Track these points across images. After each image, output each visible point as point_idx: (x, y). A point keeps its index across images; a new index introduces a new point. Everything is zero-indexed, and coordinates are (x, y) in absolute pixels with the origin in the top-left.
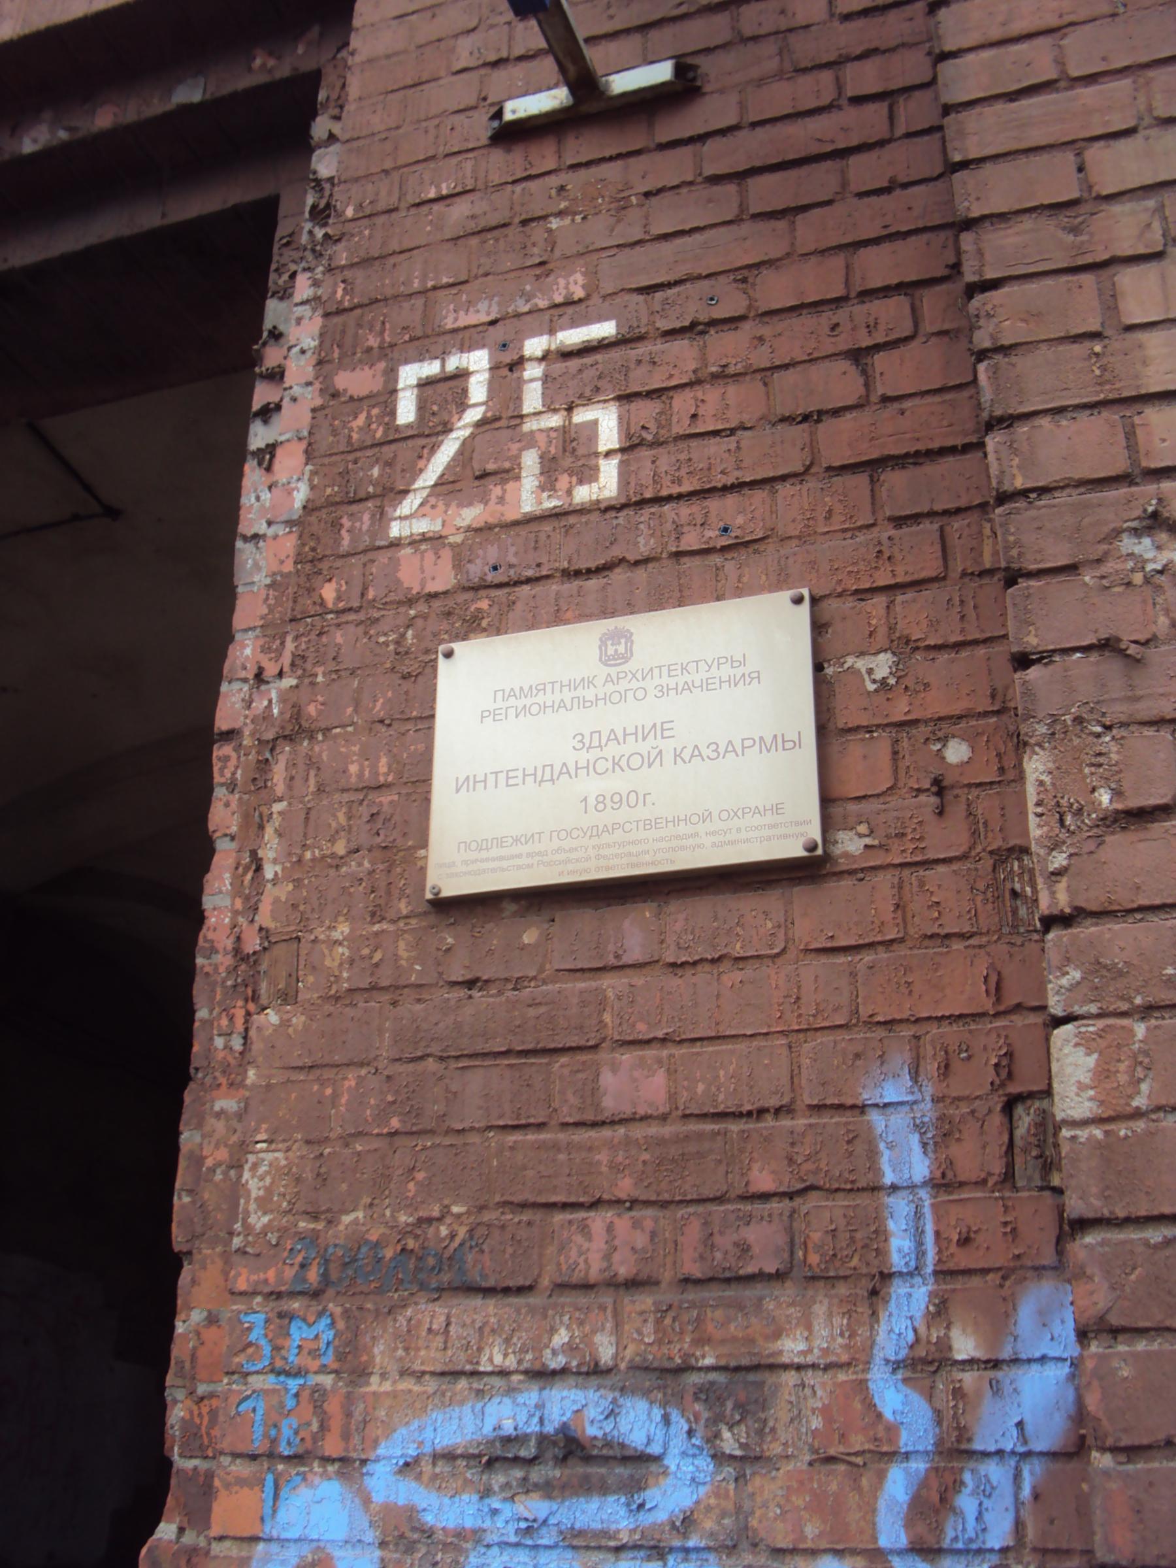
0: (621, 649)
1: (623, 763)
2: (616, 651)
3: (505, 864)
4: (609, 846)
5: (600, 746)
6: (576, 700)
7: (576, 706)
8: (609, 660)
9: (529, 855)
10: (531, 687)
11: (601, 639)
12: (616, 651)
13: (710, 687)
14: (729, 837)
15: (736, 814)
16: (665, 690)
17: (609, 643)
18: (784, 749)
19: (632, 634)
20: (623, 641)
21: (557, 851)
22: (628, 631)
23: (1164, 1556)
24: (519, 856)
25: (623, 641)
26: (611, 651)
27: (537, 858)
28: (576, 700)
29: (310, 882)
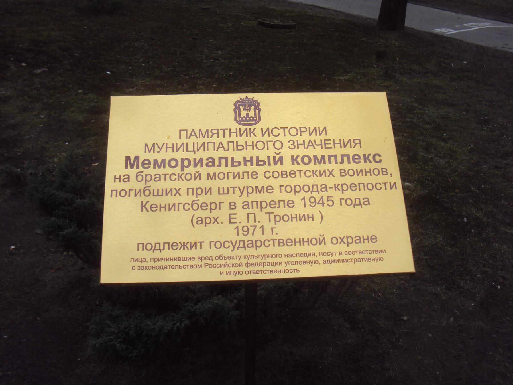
0: (252, 113)
2: (247, 115)
3: (181, 263)
4: (255, 257)
5: (194, 151)
6: (231, 144)
8: (242, 120)
9: (199, 258)
10: (207, 130)
11: (235, 104)
12: (247, 115)
13: (327, 146)
14: (334, 257)
15: (342, 240)
16: (296, 144)
17: (242, 108)
19: (259, 104)
20: (252, 108)
21: (219, 258)
24: (193, 259)
25: (252, 108)
26: (243, 114)
27: (205, 261)
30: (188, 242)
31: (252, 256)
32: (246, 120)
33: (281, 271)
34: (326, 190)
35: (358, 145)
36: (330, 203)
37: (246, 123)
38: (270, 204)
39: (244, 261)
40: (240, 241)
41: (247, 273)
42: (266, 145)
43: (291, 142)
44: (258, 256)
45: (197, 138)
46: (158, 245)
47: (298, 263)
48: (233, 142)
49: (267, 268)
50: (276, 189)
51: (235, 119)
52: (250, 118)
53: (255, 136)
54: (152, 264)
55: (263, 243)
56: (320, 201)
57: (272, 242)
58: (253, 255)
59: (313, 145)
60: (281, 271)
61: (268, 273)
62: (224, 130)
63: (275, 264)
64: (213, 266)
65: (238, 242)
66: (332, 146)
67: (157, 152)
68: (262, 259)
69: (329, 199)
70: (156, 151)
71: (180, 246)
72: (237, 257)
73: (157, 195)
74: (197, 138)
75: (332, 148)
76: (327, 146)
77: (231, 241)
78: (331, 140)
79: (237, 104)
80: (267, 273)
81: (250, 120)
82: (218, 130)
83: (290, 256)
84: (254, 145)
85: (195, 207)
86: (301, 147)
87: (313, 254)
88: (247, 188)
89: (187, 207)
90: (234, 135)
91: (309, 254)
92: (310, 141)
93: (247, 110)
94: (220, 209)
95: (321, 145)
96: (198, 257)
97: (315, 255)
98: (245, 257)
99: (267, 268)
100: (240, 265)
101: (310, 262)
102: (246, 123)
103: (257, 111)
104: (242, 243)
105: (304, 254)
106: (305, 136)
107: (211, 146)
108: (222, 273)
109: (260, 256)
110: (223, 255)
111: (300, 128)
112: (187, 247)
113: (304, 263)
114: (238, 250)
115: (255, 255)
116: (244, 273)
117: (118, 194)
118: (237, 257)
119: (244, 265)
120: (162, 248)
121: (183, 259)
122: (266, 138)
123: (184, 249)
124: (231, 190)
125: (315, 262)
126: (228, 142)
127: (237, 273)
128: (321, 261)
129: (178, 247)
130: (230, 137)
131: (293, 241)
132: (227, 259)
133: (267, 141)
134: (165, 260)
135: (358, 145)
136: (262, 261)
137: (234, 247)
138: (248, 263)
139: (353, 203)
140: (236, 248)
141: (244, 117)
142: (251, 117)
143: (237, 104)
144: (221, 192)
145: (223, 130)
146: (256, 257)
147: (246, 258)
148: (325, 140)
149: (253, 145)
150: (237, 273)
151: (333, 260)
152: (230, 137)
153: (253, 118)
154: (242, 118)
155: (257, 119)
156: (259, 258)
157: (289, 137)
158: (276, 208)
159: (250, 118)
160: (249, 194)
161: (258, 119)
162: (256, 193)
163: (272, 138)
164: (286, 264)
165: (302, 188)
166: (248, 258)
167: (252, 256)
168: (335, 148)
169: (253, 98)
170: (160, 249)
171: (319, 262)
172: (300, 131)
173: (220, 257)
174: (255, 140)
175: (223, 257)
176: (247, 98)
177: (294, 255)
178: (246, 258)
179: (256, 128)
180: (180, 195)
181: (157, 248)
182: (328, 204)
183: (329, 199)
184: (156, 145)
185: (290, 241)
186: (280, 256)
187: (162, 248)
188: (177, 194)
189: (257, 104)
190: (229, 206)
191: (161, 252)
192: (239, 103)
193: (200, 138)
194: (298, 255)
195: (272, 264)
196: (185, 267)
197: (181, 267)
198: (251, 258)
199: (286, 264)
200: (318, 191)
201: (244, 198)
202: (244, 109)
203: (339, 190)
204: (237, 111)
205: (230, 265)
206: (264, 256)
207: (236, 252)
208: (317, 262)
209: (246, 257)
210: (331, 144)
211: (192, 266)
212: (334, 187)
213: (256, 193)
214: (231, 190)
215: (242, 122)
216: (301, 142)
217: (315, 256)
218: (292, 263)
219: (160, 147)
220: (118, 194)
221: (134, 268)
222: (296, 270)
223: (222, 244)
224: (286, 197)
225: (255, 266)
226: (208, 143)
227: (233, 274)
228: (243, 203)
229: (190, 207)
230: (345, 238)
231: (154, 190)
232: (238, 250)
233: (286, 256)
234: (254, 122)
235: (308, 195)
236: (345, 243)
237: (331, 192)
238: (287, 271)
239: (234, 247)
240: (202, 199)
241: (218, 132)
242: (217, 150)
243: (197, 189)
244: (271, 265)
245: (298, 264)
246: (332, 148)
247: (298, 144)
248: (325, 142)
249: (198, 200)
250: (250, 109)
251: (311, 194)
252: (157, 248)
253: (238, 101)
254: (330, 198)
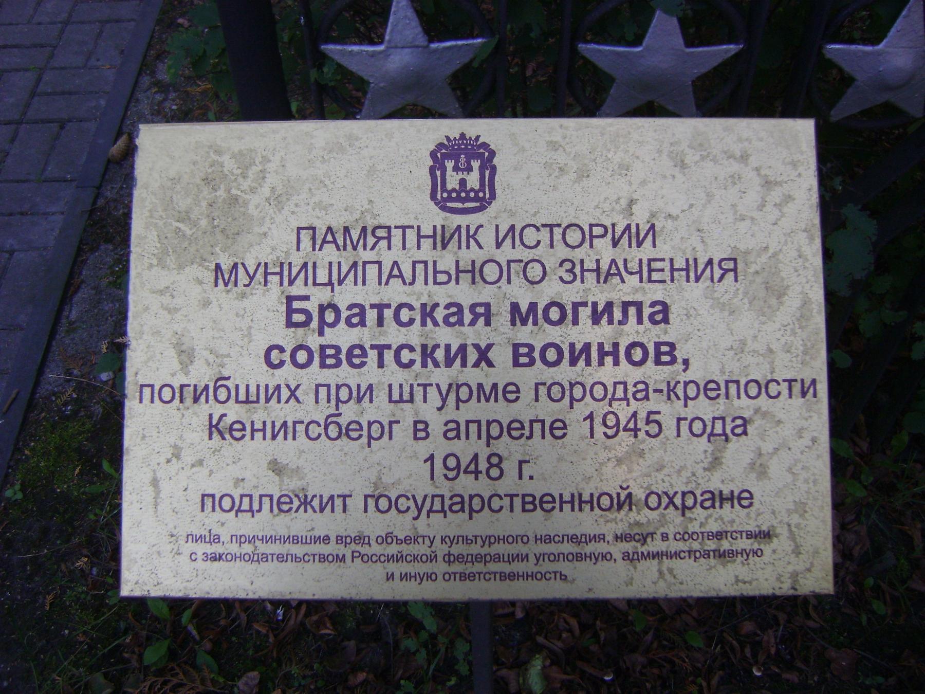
0: (473, 180)
1: (665, 500)
2: (463, 182)
5: (330, 283)
6: (420, 268)
7: (420, 278)
8: (450, 199)
11: (433, 155)
12: (463, 182)
17: (450, 164)
18: (435, 283)
19: (493, 154)
22: (485, 145)
23: (431, 613)
25: (476, 164)
26: (453, 181)
27: (353, 546)
28: (420, 268)
29: (33, 450)
30: (315, 496)
31: (460, 539)
32: (459, 199)
33: (527, 576)
34: (647, 398)
35: (731, 275)
36: (654, 429)
37: (459, 205)
38: (509, 429)
39: (441, 549)
40: (433, 496)
41: (447, 577)
42: (505, 273)
43: (568, 266)
44: (473, 539)
46: (246, 500)
47: (566, 557)
48: (425, 263)
49: (493, 567)
50: (527, 394)
51: (433, 196)
52: (467, 193)
53: (480, 247)
54: (234, 548)
55: (486, 503)
56: (628, 422)
57: (507, 500)
58: (463, 537)
59: (619, 274)
60: (527, 576)
61: (495, 580)
62: (404, 228)
63: (511, 560)
64: (370, 558)
65: (429, 500)
66: (666, 275)
67: (245, 286)
68: (482, 547)
69: (650, 419)
70: (240, 283)
71: (296, 503)
72: (427, 539)
73: (244, 399)
75: (664, 281)
76: (655, 276)
77: (414, 497)
78: (663, 260)
79: (439, 155)
80: (493, 579)
81: (467, 199)
82: (389, 228)
83: (547, 541)
84: (475, 273)
85: (333, 431)
86: (590, 277)
87: (601, 538)
88: (459, 387)
89: (314, 430)
90: (427, 244)
91: (592, 536)
92: (613, 261)
93: (463, 170)
94: (391, 438)
95: (640, 272)
96: (337, 537)
97: (606, 540)
98: (443, 540)
99: (493, 567)
100: (433, 558)
101: (593, 556)
102: (459, 205)
103: (487, 173)
104: (437, 501)
105: (579, 537)
106: (604, 251)
107: (372, 270)
108: (390, 577)
109: (479, 539)
110: (394, 534)
111: (591, 226)
112: (312, 507)
113: (579, 557)
114: (428, 517)
115: (467, 537)
116: (440, 577)
117: (156, 395)
118: (427, 539)
119: (440, 559)
120: (256, 506)
121: (304, 541)
122: (507, 253)
123: (306, 511)
124: (419, 393)
125: (604, 557)
126: (414, 263)
127: (425, 578)
128: (618, 555)
129: (291, 506)
130: (419, 247)
131: (558, 500)
132: (403, 544)
133: (509, 262)
134: (262, 540)
135: (731, 275)
136: (483, 551)
137: (420, 511)
138: (449, 555)
139: (709, 430)
140: (424, 512)
141: (454, 190)
142: (472, 190)
143: (439, 155)
144: (396, 397)
145: (401, 230)
146: (469, 542)
147: (446, 543)
148: (650, 261)
149: (473, 271)
150: (425, 578)
151: (646, 554)
152: (419, 247)
153: (476, 192)
154: (450, 192)
155: (485, 194)
156: (476, 543)
157: (562, 252)
158: (524, 438)
159: (467, 193)
160: (460, 403)
161: (487, 196)
162: (479, 401)
163: (521, 253)
164: (538, 560)
165: (588, 389)
166: (452, 543)
167: (460, 539)
168: (672, 280)
169: (478, 137)
170: (251, 510)
171: (613, 557)
172: (589, 237)
173: (388, 538)
174: (477, 255)
175: (395, 539)
176: (463, 136)
177: (557, 539)
178: (446, 543)
179: (482, 226)
180: (298, 401)
181: (246, 506)
182: (647, 433)
183: (650, 419)
184: (240, 266)
185: (550, 499)
186: (525, 539)
187: (256, 506)
188: (292, 400)
189: (487, 154)
190: (411, 430)
191: (253, 516)
192: (444, 151)
193: (345, 249)
194: (565, 538)
195: (506, 559)
196: (307, 558)
197: (300, 558)
198: (457, 543)
199: (538, 560)
200: (626, 398)
201: (450, 413)
202: (456, 169)
203: (678, 398)
204: (438, 173)
205: (409, 558)
206: (488, 540)
207: (422, 525)
208: (608, 557)
209: (447, 540)
210: (662, 270)
211: (323, 558)
212: (665, 390)
213: (479, 401)
214: (419, 393)
215: (449, 204)
216: (590, 264)
217: (604, 541)
218: (552, 558)
219: (251, 274)
220: (156, 395)
221: (194, 557)
222: (558, 575)
223: (393, 503)
224: (547, 410)
225: (467, 561)
226: (365, 263)
227: (416, 580)
228: (446, 424)
229: (321, 430)
230: (679, 496)
231: (237, 387)
232: (428, 517)
233: (539, 542)
234: (478, 204)
235: (601, 409)
236: (676, 508)
237: (655, 403)
238: (539, 576)
239: (420, 511)
240: (349, 413)
241: (389, 232)
242: (387, 283)
243: (338, 387)
244: (503, 561)
245: (564, 560)
246: (664, 281)
247: (583, 270)
248: (649, 265)
249: (340, 415)
250: (469, 169)
251: (610, 405)
252: (246, 506)
253: (440, 146)
254: (653, 417)
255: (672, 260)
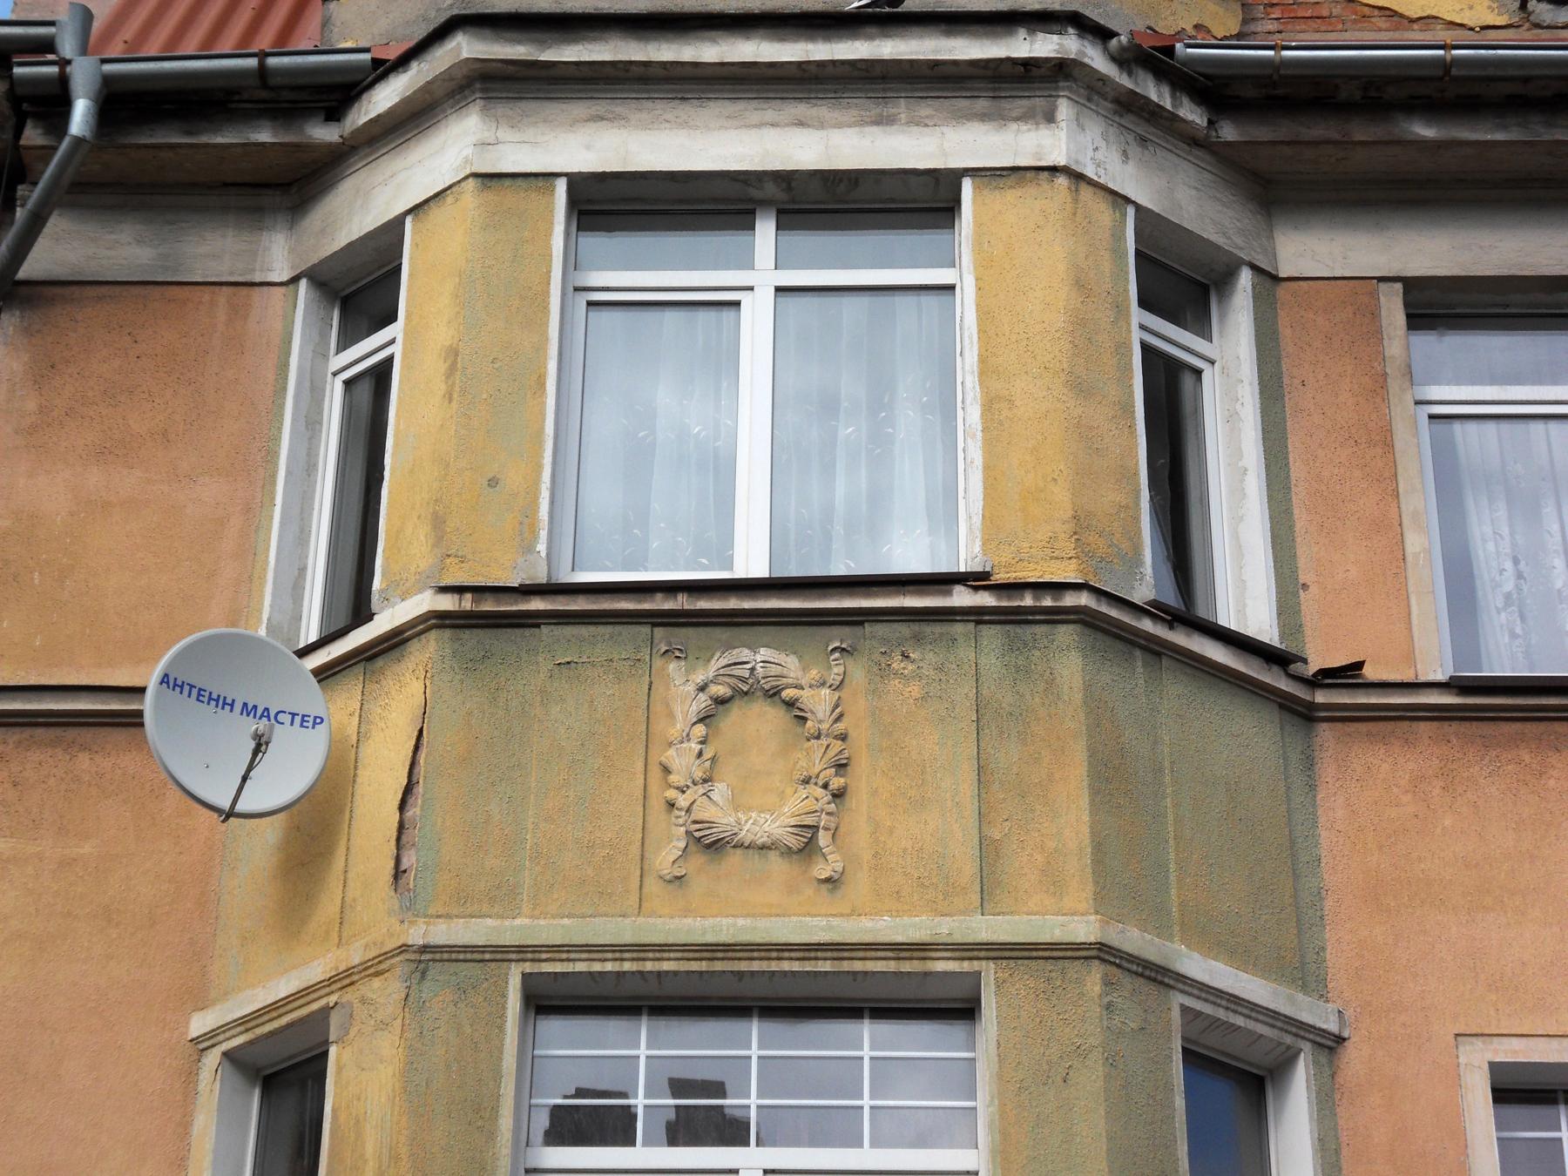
13: (201, 698)
45: (169, 687)
66: (206, 700)
74: (169, 687)
75: (203, 702)
246: (203, 702)
255: (211, 693)
